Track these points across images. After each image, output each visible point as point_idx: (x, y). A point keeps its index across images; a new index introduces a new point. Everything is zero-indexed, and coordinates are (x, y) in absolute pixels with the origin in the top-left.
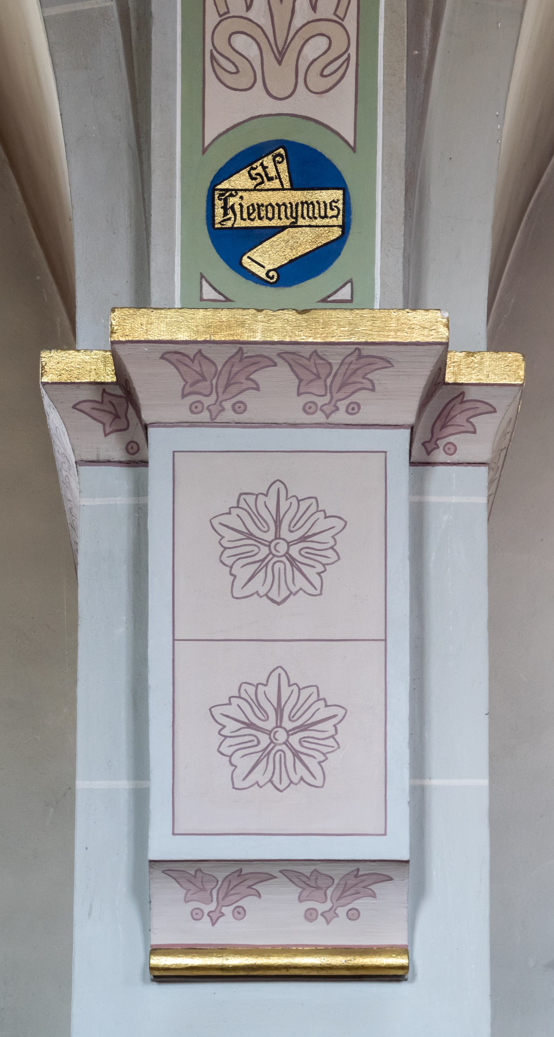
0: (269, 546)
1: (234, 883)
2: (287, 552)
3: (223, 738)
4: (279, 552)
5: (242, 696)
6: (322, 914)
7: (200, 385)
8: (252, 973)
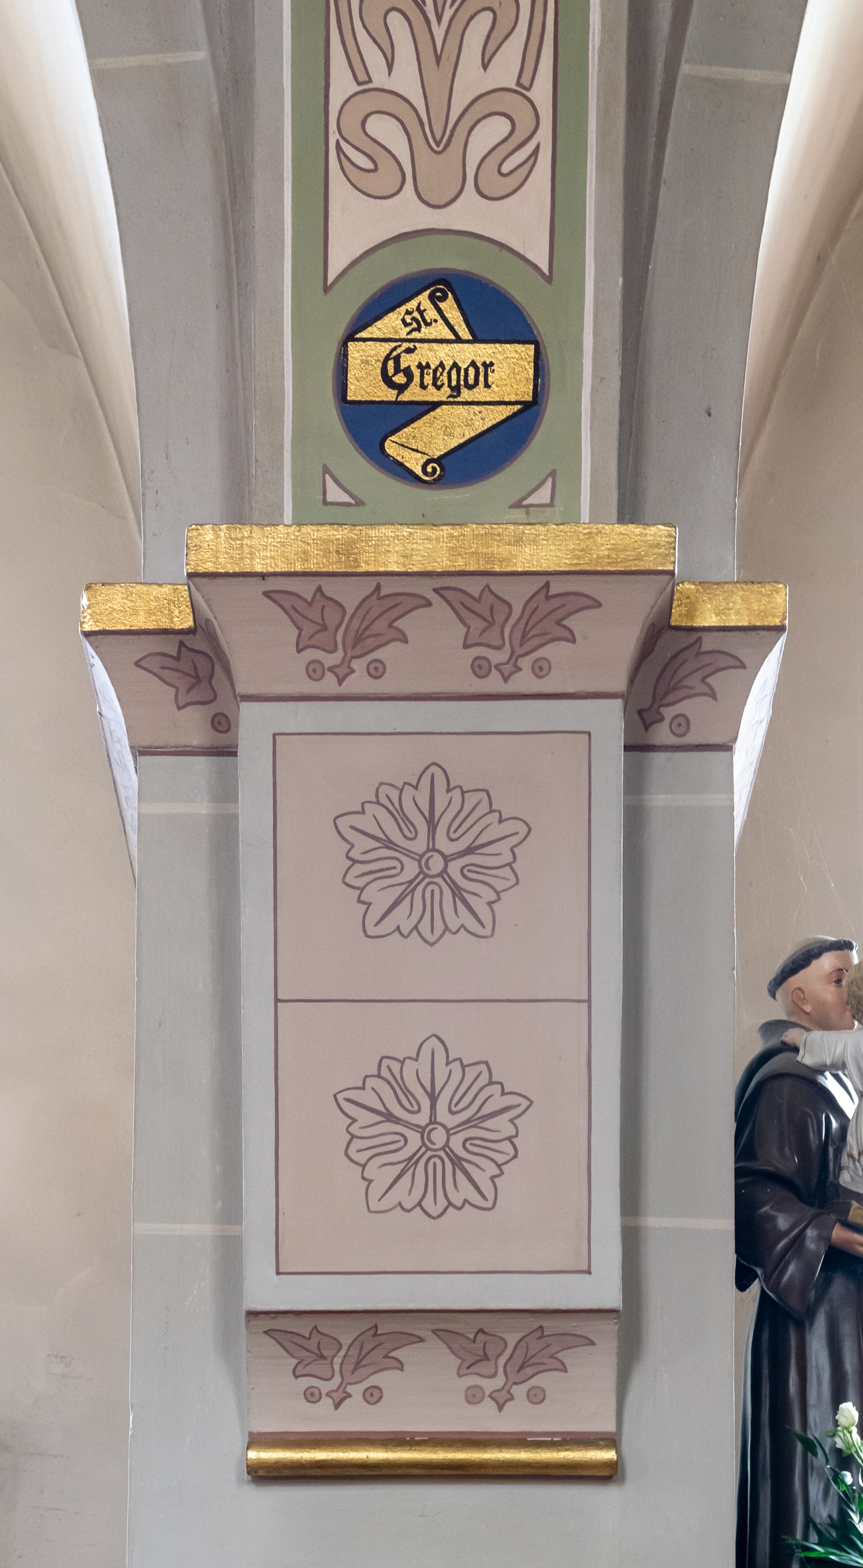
0: (419, 861)
1: (367, 1347)
2: (447, 1144)
3: (351, 863)
4: (434, 1144)
5: (381, 801)
6: (497, 667)
7: (319, 636)
8: (393, 1472)
